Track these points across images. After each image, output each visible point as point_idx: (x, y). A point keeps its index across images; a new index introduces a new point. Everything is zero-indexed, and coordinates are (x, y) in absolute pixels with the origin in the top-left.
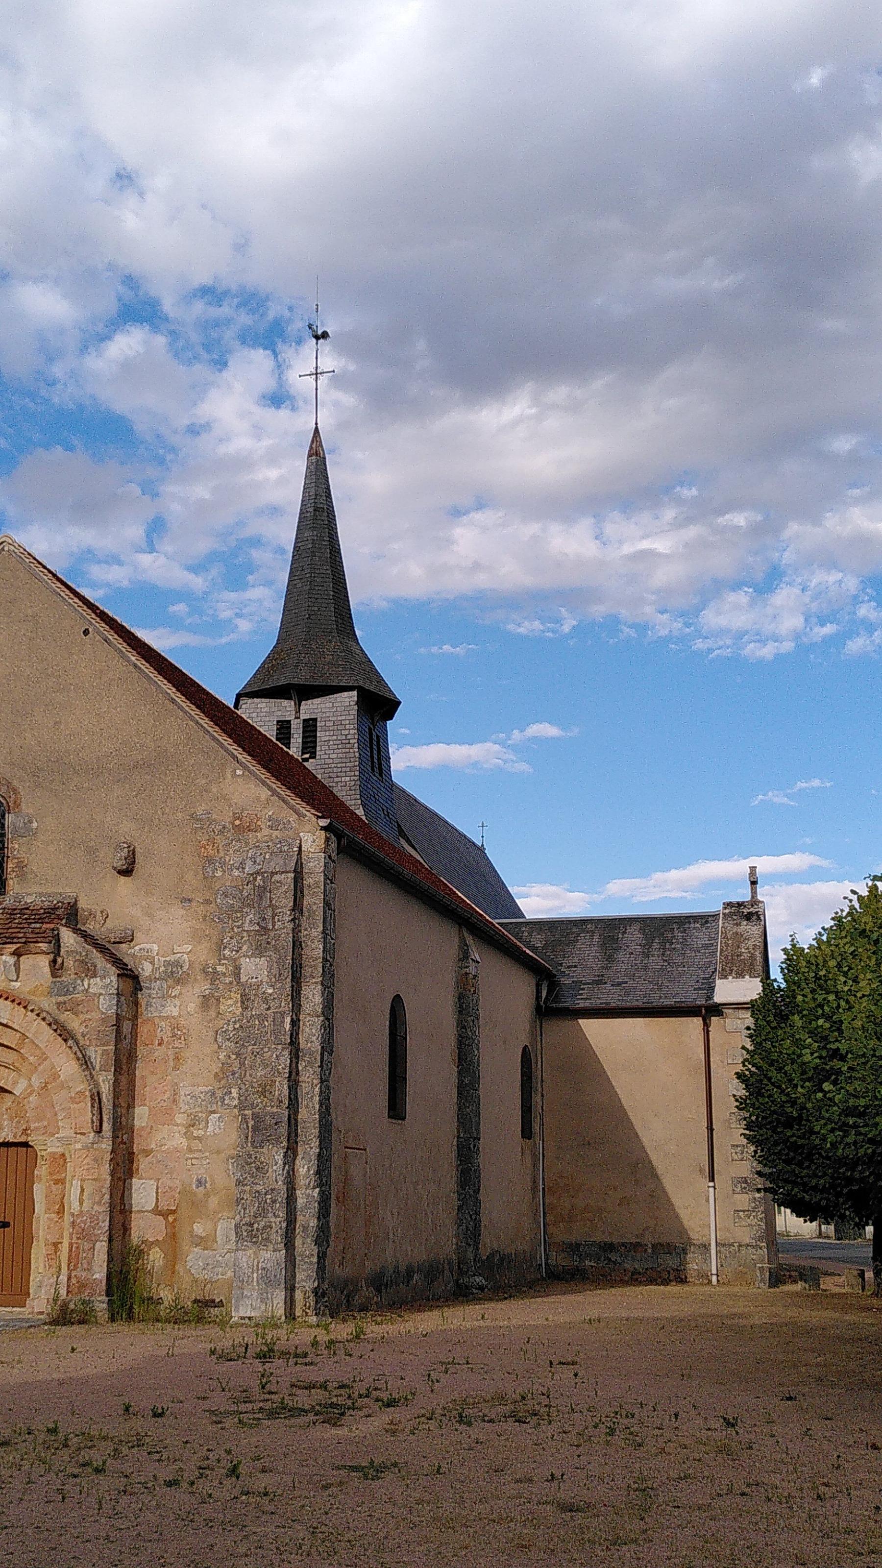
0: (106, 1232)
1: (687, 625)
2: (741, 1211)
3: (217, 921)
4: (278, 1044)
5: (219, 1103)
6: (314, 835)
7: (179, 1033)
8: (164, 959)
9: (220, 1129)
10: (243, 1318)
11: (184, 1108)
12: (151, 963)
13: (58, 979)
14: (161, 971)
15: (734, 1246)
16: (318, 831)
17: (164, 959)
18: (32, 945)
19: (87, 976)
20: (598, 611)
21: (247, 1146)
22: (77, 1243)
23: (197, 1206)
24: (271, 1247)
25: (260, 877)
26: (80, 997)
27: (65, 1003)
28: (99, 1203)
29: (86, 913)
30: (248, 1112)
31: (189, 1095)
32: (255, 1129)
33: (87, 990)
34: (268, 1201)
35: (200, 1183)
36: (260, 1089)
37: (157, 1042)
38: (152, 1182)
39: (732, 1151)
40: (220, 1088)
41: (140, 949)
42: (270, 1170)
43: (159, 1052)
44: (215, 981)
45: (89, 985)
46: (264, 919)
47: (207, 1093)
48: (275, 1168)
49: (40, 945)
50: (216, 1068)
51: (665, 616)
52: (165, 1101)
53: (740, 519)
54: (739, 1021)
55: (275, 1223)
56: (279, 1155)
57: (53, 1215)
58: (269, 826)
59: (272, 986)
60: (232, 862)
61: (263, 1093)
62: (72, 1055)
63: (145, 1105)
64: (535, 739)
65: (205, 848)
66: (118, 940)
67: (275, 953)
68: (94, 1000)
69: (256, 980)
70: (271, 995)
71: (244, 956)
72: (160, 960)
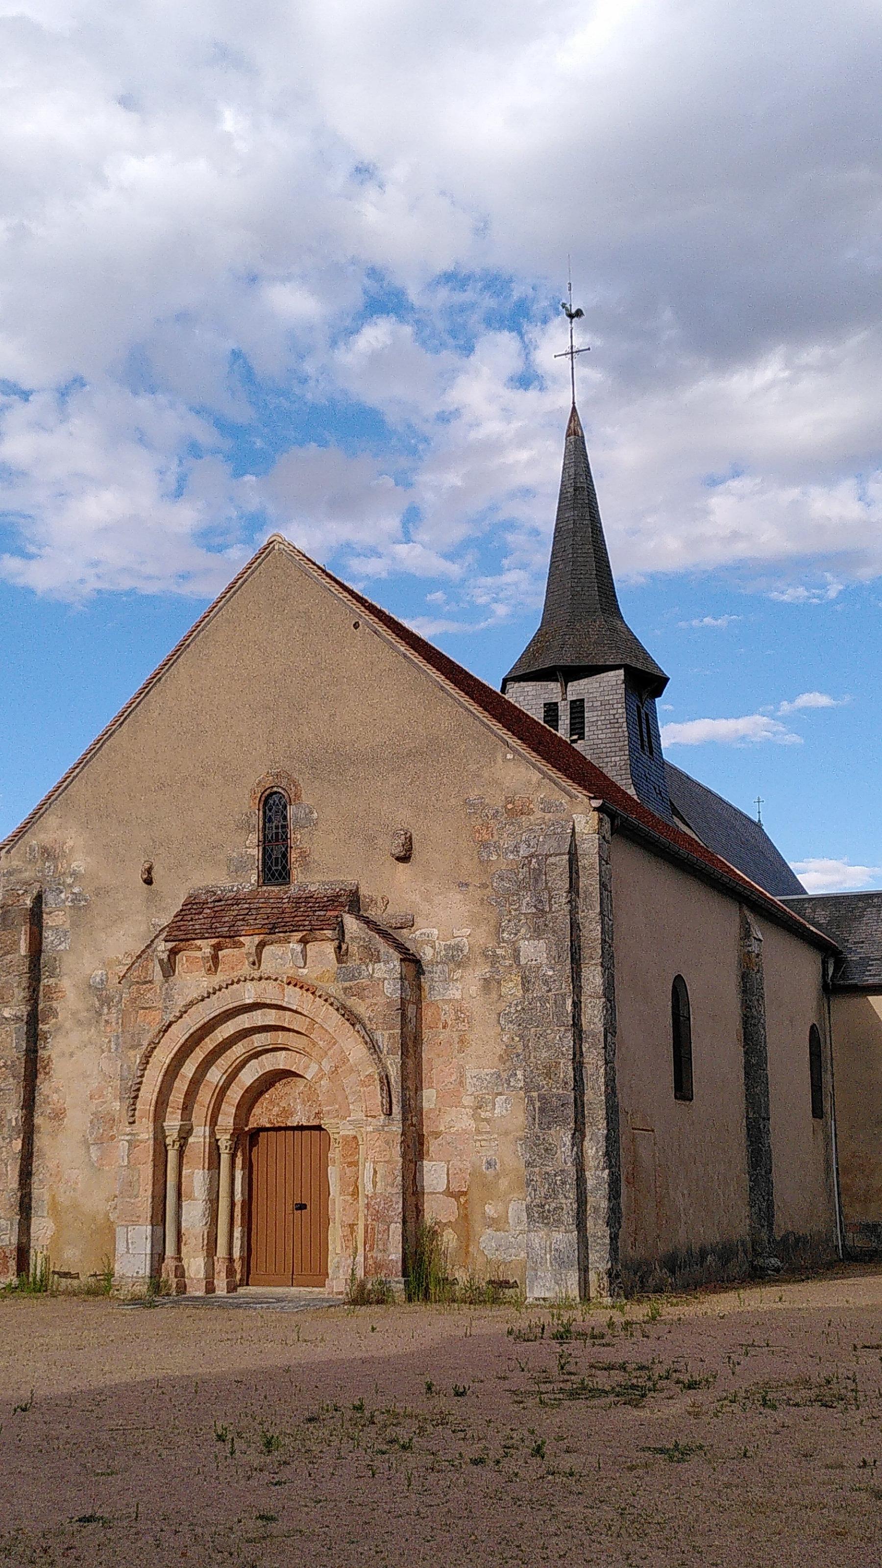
3: (495, 904)
7: (462, 1015)
9: (507, 1110)
10: (537, 1299)
11: (471, 1090)
12: (432, 947)
13: (344, 965)
17: (444, 943)
18: (317, 932)
19: (371, 961)
21: (535, 1127)
27: (351, 988)
29: (367, 900)
30: (535, 1094)
31: (475, 1077)
32: (542, 1110)
38: (443, 1164)
42: (559, 1151)
45: (373, 970)
46: (541, 901)
49: (325, 932)
50: (499, 1050)
52: (451, 1083)
55: (566, 1204)
59: (551, 968)
60: (506, 846)
61: (548, 1075)
63: (432, 1087)
66: (399, 925)
67: (554, 935)
68: (378, 984)
70: (551, 977)
72: (440, 945)
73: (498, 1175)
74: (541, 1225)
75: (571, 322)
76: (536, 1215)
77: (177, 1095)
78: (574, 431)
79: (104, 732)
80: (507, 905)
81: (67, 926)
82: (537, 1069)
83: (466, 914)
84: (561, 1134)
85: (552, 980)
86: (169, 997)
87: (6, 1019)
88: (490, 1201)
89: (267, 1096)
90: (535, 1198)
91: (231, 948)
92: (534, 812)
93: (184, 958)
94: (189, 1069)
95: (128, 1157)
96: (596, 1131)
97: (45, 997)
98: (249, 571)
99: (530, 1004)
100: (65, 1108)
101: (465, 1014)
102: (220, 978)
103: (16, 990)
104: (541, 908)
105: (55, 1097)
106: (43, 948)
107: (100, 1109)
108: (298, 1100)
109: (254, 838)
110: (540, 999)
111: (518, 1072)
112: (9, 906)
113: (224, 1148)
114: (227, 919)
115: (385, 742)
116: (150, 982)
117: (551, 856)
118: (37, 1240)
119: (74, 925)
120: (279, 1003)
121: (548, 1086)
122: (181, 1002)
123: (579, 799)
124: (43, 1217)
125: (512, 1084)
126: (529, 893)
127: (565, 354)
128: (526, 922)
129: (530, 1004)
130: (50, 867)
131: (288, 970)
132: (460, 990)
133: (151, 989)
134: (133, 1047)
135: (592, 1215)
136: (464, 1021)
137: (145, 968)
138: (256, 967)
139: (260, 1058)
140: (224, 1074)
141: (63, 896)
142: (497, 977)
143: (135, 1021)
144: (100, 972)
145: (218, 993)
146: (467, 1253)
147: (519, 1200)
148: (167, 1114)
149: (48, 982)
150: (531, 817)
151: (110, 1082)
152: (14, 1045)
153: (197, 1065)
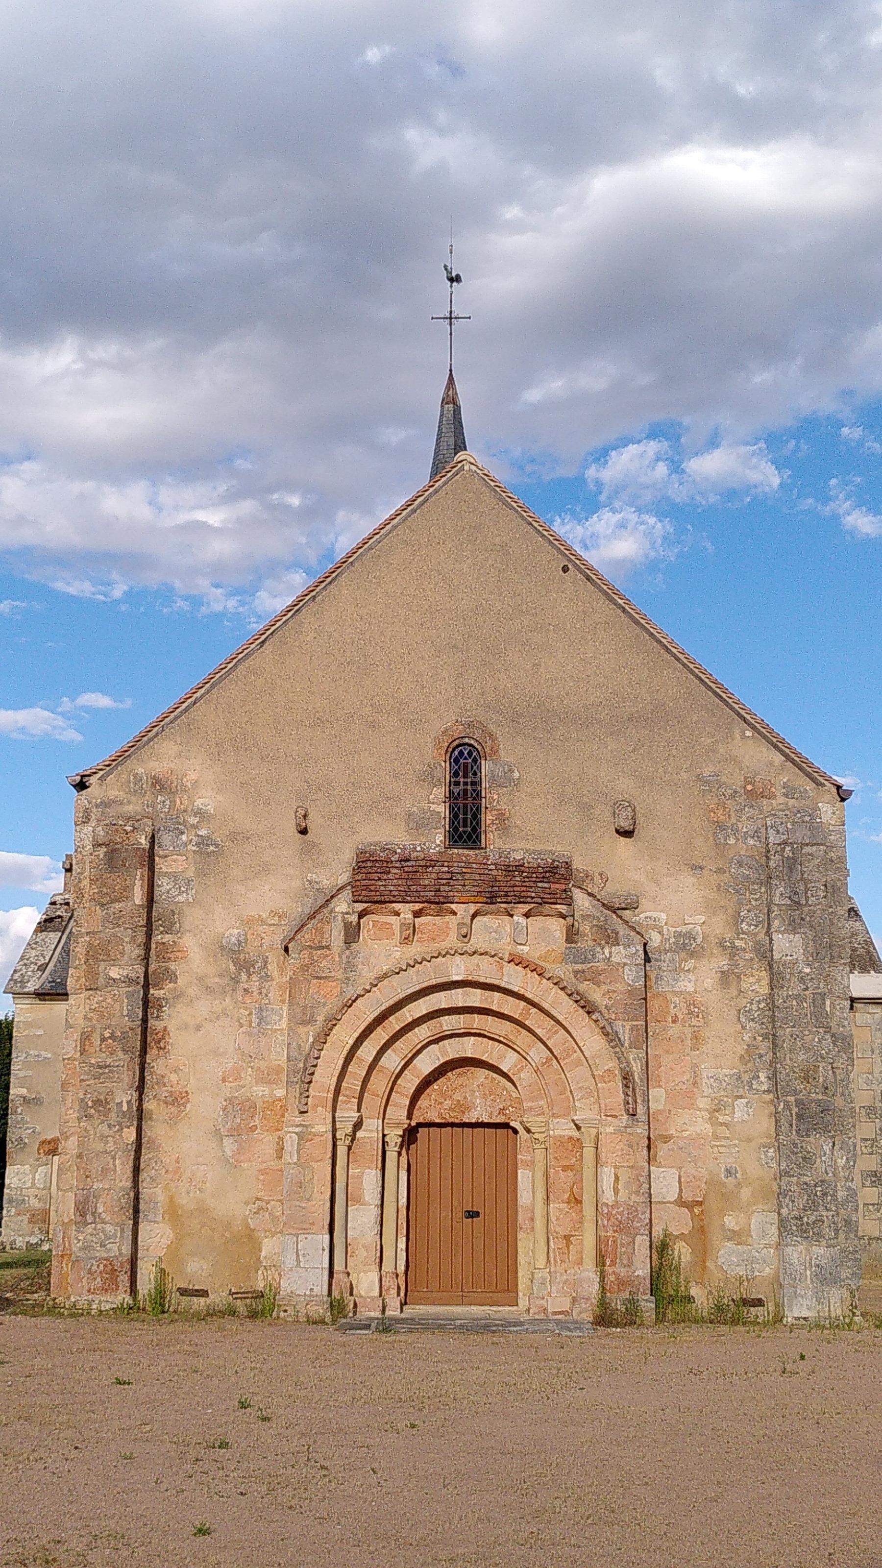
0: (646, 1225)
1: (242, 603)
2: (871, 1204)
3: (733, 892)
4: (820, 1027)
5: (746, 1087)
6: (834, 807)
7: (696, 1010)
8: (674, 929)
9: (749, 1115)
10: (796, 1318)
11: (707, 1091)
12: (660, 933)
13: (573, 945)
14: (671, 942)
15: (864, 1239)
16: (838, 803)
17: (674, 929)
18: (547, 905)
19: (608, 943)
20: (152, 579)
21: (792, 1134)
22: (613, 1237)
23: (729, 1199)
24: (824, 1243)
25: (790, 848)
26: (601, 965)
27: (583, 972)
28: (637, 1193)
29: (582, 875)
30: (791, 1099)
31: (712, 1077)
32: (800, 1116)
33: (609, 959)
34: (818, 1193)
35: (729, 1172)
36: (802, 1075)
37: (670, 1019)
38: (674, 1170)
39: (862, 1144)
40: (747, 1071)
41: (646, 918)
42: (818, 1160)
43: (674, 1030)
44: (734, 956)
45: (610, 953)
46: (796, 893)
47: (732, 1076)
48: (823, 1158)
49: (558, 906)
50: (741, 1049)
51: (220, 590)
52: (684, 1083)
53: (295, 501)
54: (869, 1016)
55: (827, 1217)
56: (827, 1145)
57: (562, 1206)
58: (784, 793)
59: (808, 965)
60: (745, 830)
61: (806, 1079)
62: (597, 1030)
63: (660, 1086)
64: (86, 709)
65: (715, 813)
66: (623, 906)
67: (811, 931)
68: (618, 970)
69: (791, 958)
70: (808, 975)
71: (776, 931)
72: (669, 931)
73: (739, 1184)
74: (799, 1239)
75: (451, 286)
76: (794, 1228)
77: (352, 1081)
78: (453, 400)
79: (240, 651)
80: (747, 894)
81: (190, 873)
82: (794, 1072)
83: (701, 900)
84: (821, 1141)
85: (809, 977)
86: (350, 966)
87: (114, 980)
88: (731, 1213)
89: (436, 1087)
90: (793, 1210)
91: (432, 915)
92: (775, 796)
93: (371, 923)
94: (368, 1052)
95: (298, 1153)
96: (847, 1139)
97: (158, 956)
98: (432, 489)
99: (785, 1002)
100: (187, 1092)
101: (699, 1008)
102: (415, 950)
103: (128, 947)
104: (797, 900)
105: (174, 1077)
106: (155, 899)
107: (236, 1094)
108: (477, 1094)
109: (440, 792)
110: (797, 997)
111: (761, 1074)
112: (117, 843)
113: (394, 1144)
114: (427, 882)
115: (601, 702)
116: (328, 947)
117: (807, 845)
118: (147, 1250)
119: (202, 873)
120: (496, 982)
121: (806, 1090)
122: (367, 975)
123: (826, 788)
124: (155, 1222)
125: (754, 1087)
126: (783, 883)
127: (444, 318)
128: (780, 914)
129: (785, 1002)
130: (164, 802)
131: (506, 947)
132: (692, 983)
133: (327, 956)
134: (304, 1023)
135: (843, 1228)
136: (698, 1016)
137: (320, 932)
138: (466, 940)
139: (440, 1043)
140: (403, 1059)
141: (184, 838)
142: (736, 970)
143: (307, 993)
144: (236, 931)
145: (417, 966)
146: (704, 1268)
147: (764, 1211)
148: (339, 1103)
149: (162, 938)
150: (773, 802)
151: (250, 1062)
152: (125, 1013)
153: (379, 1048)
